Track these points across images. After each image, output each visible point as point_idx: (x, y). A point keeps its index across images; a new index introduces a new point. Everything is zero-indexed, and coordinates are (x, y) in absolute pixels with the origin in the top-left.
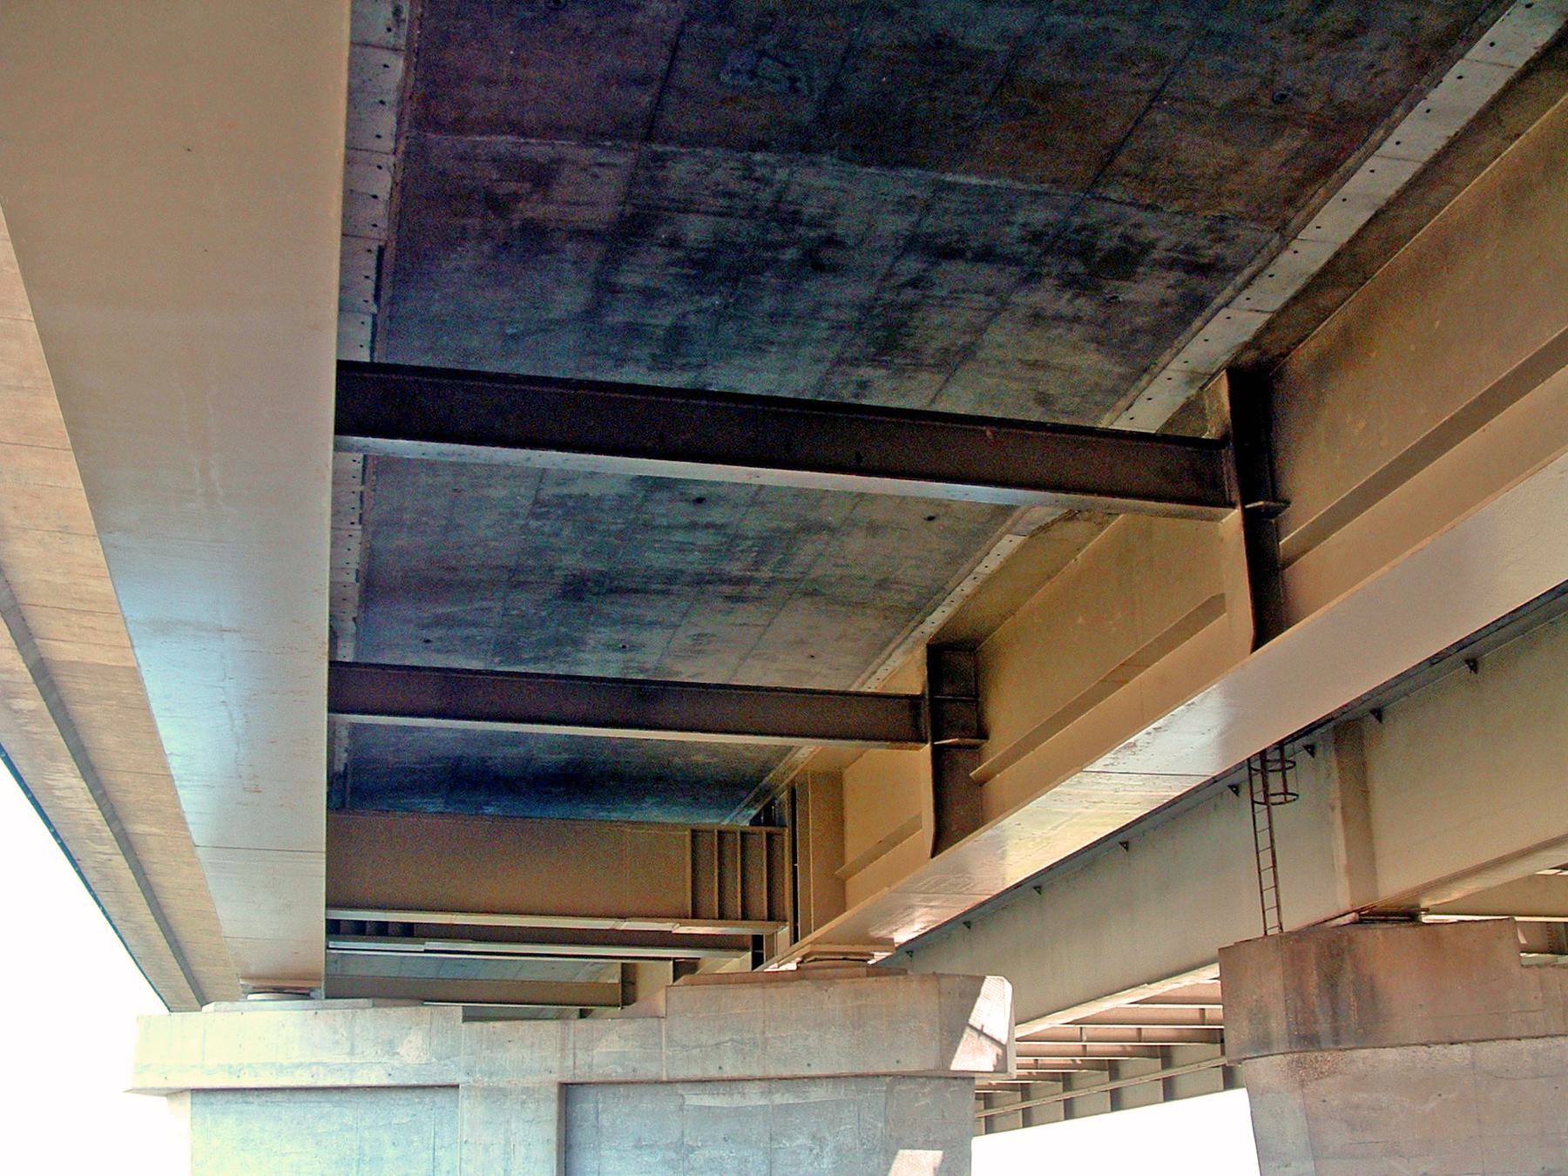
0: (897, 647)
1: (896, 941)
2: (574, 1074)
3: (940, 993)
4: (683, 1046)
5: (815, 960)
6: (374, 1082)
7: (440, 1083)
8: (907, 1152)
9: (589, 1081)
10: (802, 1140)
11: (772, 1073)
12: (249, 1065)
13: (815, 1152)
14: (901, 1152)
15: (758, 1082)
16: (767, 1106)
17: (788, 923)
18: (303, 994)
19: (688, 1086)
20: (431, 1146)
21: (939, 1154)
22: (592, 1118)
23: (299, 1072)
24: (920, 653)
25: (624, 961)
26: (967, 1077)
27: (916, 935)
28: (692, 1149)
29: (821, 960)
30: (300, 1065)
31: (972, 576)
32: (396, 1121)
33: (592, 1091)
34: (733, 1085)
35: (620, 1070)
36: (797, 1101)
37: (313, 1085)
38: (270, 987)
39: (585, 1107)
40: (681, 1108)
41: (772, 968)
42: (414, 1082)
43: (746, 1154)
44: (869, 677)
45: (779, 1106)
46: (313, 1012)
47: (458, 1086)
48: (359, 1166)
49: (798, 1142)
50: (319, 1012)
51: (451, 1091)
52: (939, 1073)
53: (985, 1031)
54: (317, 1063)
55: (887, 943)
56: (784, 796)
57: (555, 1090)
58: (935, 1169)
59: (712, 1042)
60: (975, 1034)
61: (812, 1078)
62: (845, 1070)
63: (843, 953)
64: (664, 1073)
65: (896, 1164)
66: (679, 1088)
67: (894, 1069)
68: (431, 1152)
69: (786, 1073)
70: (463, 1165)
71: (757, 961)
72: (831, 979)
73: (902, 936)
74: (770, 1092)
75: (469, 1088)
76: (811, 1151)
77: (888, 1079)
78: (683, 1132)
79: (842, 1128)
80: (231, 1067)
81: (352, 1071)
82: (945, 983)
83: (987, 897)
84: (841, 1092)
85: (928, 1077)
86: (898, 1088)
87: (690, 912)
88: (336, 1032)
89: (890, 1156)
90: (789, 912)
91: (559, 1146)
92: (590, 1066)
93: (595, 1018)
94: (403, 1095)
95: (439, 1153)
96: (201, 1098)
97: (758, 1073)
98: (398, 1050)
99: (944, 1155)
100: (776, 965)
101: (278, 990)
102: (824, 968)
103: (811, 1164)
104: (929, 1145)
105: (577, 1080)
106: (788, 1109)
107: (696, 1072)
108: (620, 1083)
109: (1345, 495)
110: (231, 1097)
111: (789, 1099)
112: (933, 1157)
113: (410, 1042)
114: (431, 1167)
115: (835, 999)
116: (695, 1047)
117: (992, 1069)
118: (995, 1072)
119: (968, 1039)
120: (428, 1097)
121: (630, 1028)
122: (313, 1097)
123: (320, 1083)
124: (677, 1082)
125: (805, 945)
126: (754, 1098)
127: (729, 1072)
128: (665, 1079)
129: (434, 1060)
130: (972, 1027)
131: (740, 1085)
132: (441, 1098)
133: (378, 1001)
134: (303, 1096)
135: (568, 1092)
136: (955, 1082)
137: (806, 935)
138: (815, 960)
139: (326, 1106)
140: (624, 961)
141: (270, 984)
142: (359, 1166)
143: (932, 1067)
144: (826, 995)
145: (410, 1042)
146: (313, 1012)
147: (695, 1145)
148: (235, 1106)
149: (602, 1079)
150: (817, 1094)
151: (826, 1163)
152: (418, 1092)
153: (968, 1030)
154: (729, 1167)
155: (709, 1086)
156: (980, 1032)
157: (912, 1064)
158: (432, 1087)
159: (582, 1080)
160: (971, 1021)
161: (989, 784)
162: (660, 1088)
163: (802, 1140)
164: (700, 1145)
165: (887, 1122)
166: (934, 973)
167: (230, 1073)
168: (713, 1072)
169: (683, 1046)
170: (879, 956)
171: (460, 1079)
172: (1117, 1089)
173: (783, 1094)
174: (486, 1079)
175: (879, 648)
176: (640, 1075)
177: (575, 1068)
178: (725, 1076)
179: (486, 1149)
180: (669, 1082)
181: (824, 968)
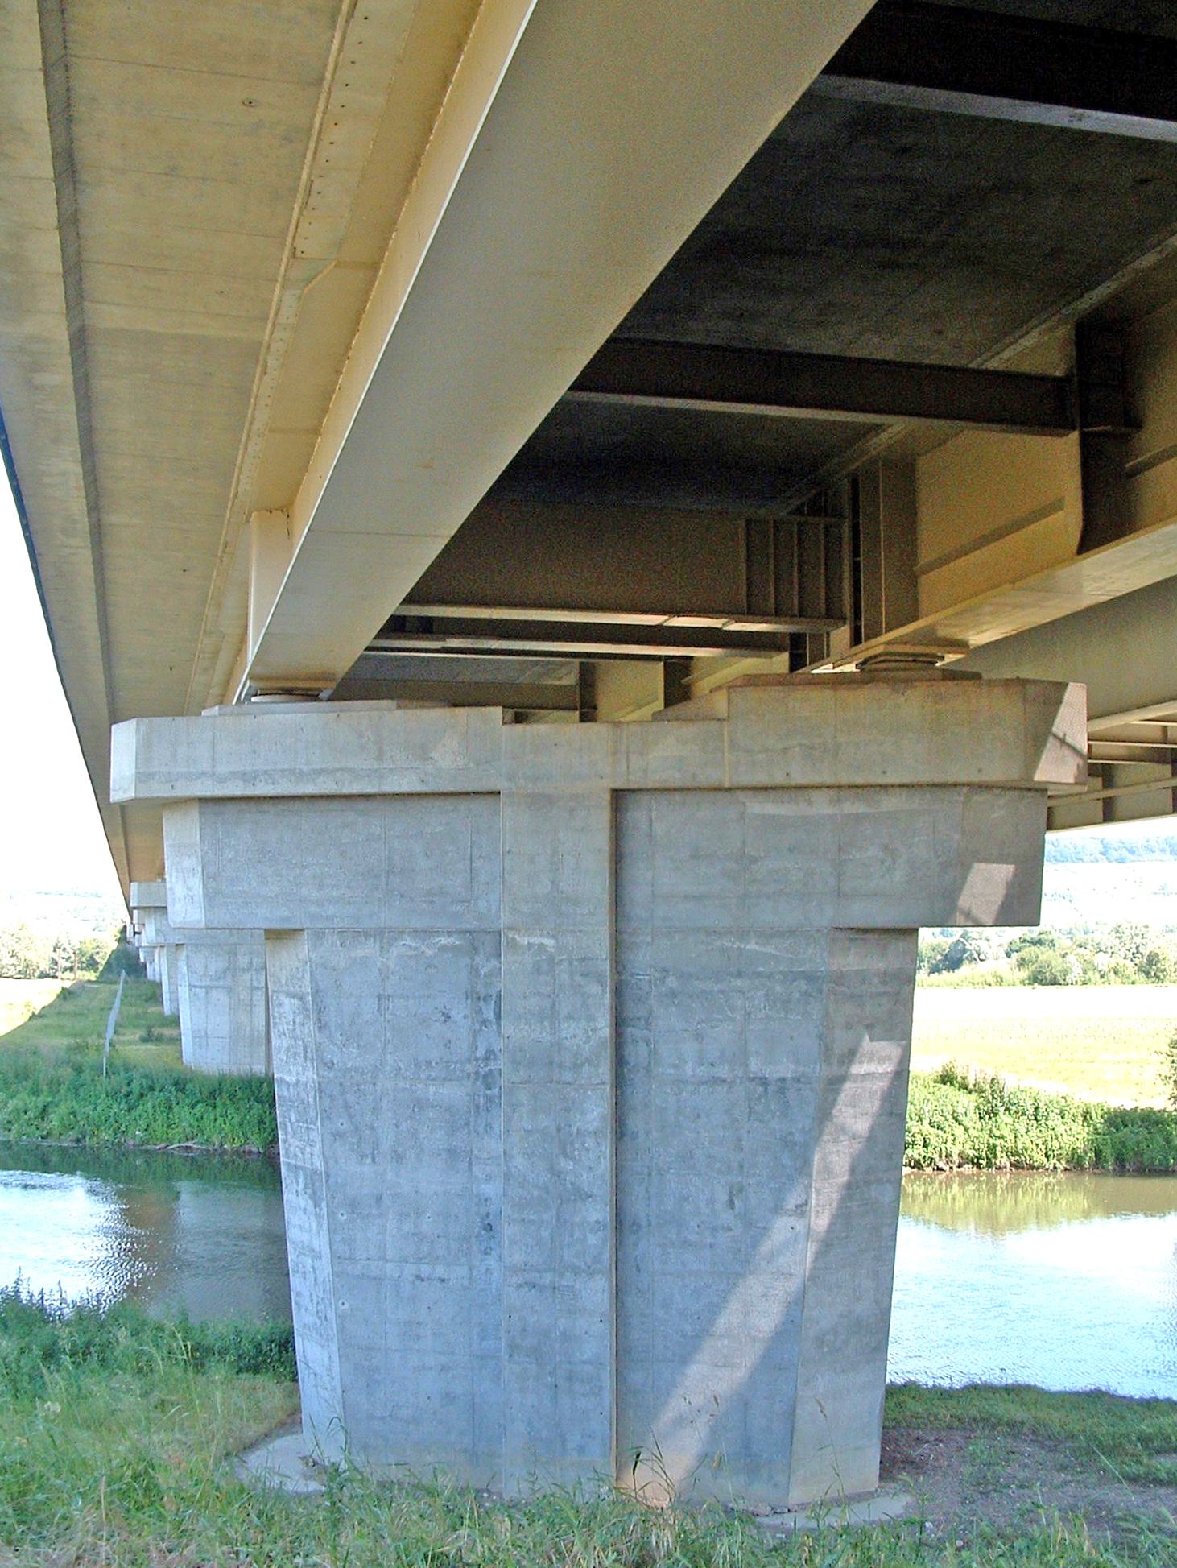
0: (1036, 326)
1: (971, 642)
2: (628, 780)
3: (1025, 700)
4: (748, 751)
5: (884, 661)
6: (405, 789)
7: (479, 789)
8: (983, 866)
9: (643, 786)
10: (872, 852)
11: (844, 779)
12: (265, 772)
13: (887, 864)
14: (976, 866)
15: (826, 790)
16: (836, 815)
17: (848, 622)
18: (311, 696)
19: (750, 793)
20: (468, 857)
21: (1011, 867)
22: (645, 827)
23: (321, 779)
24: (1065, 331)
25: (583, 660)
26: (1041, 790)
27: (1001, 636)
28: (754, 860)
29: (889, 661)
30: (321, 772)
31: (1159, 248)
32: (428, 830)
33: (645, 799)
34: (800, 793)
35: (677, 775)
36: (868, 810)
37: (338, 792)
38: (278, 689)
39: (638, 815)
40: (742, 816)
41: (826, 669)
42: (451, 789)
43: (813, 865)
44: (993, 356)
45: (848, 816)
46: (335, 715)
47: (499, 793)
48: (388, 877)
49: (869, 854)
50: (342, 714)
51: (490, 799)
52: (1024, 784)
53: (1068, 740)
54: (342, 769)
55: (959, 645)
56: (845, 485)
57: (607, 797)
58: (1007, 883)
59: (780, 746)
60: (1058, 743)
61: (884, 787)
62: (924, 778)
63: (913, 655)
64: (727, 779)
65: (971, 878)
66: (742, 796)
67: (975, 778)
68: (468, 862)
69: (860, 781)
70: (506, 876)
71: (796, 663)
72: (909, 682)
73: (977, 639)
74: (839, 800)
75: (511, 794)
76: (882, 863)
77: (965, 789)
78: (744, 842)
79: (917, 839)
80: (245, 774)
81: (381, 777)
82: (1031, 690)
83: (1109, 598)
84: (915, 802)
85: (1004, 787)
86: (976, 798)
87: (745, 609)
88: (361, 736)
89: (966, 868)
90: (848, 610)
91: (611, 855)
92: (645, 771)
93: (537, 721)
94: (439, 803)
95: (478, 864)
96: (211, 807)
97: (828, 779)
98: (432, 755)
99: (1016, 869)
100: (831, 666)
101: (288, 692)
102: (892, 670)
103: (883, 877)
104: (1001, 859)
105: (632, 786)
106: (858, 818)
107: (762, 779)
108: (675, 790)
109: (459, 66)
110: (243, 806)
111: (861, 808)
112: (1005, 871)
113: (444, 745)
114: (469, 879)
115: (912, 704)
116: (760, 752)
117: (1072, 780)
118: (1076, 783)
119: (1051, 747)
120: (463, 805)
121: (689, 730)
122: (335, 805)
123: (346, 790)
124: (738, 788)
125: (875, 646)
126: (821, 806)
127: (798, 779)
128: (727, 785)
129: (471, 765)
130: (1055, 736)
131: (807, 792)
132: (479, 806)
133: (401, 702)
134: (323, 804)
135: (619, 797)
136: (1029, 794)
137: (891, 630)
138: (884, 661)
139: (349, 814)
140: (583, 660)
141: (280, 685)
142: (388, 877)
143: (1016, 777)
144: (903, 699)
145: (444, 745)
146: (335, 715)
147: (756, 854)
148: (248, 815)
149: (657, 785)
150: (890, 803)
151: (899, 876)
152: (451, 800)
153: (1051, 739)
154: (794, 879)
155: (773, 794)
156: (1063, 742)
157: (995, 773)
158: (468, 794)
159: (636, 786)
160: (1054, 729)
161: (1141, 477)
162: (719, 795)
163: (872, 852)
164: (762, 855)
165: (963, 833)
166: (1018, 678)
167: (244, 781)
168: (779, 779)
169: (748, 751)
170: (951, 658)
171: (500, 785)
172: (1110, 798)
173: (853, 803)
174: (530, 785)
175: (1017, 324)
176: (703, 780)
177: (629, 773)
178: (793, 783)
179: (532, 860)
180: (729, 789)
181: (892, 670)
